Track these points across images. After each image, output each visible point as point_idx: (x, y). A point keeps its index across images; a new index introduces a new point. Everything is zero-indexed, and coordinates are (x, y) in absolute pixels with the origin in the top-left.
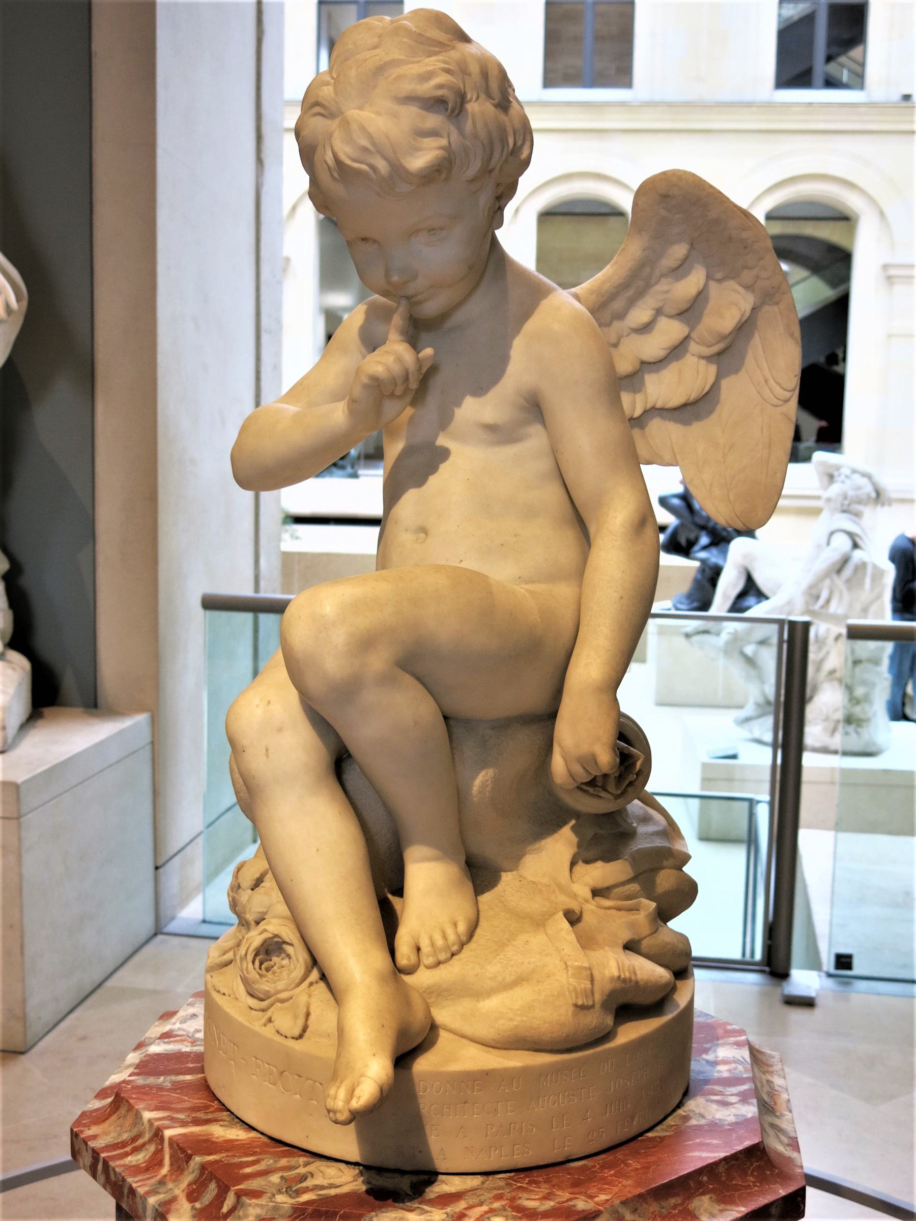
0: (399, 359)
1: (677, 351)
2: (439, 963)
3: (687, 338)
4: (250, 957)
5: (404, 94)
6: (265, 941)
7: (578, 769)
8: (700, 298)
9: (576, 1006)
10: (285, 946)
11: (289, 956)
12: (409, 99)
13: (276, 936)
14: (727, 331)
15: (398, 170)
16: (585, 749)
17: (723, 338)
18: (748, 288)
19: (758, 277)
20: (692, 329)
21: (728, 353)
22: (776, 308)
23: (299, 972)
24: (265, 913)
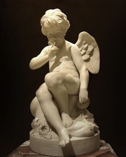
0: (55, 48)
1: (85, 54)
2: (70, 126)
3: (86, 52)
4: (40, 129)
5: (57, 15)
6: (42, 127)
7: (83, 100)
8: (87, 48)
9: (91, 129)
10: (45, 127)
11: (46, 128)
12: (58, 16)
13: (44, 126)
14: (91, 51)
15: (56, 23)
16: (84, 97)
17: (90, 52)
18: (93, 46)
19: (94, 44)
20: (86, 51)
21: (91, 54)
22: (96, 48)
23: (48, 130)
24: (40, 124)
